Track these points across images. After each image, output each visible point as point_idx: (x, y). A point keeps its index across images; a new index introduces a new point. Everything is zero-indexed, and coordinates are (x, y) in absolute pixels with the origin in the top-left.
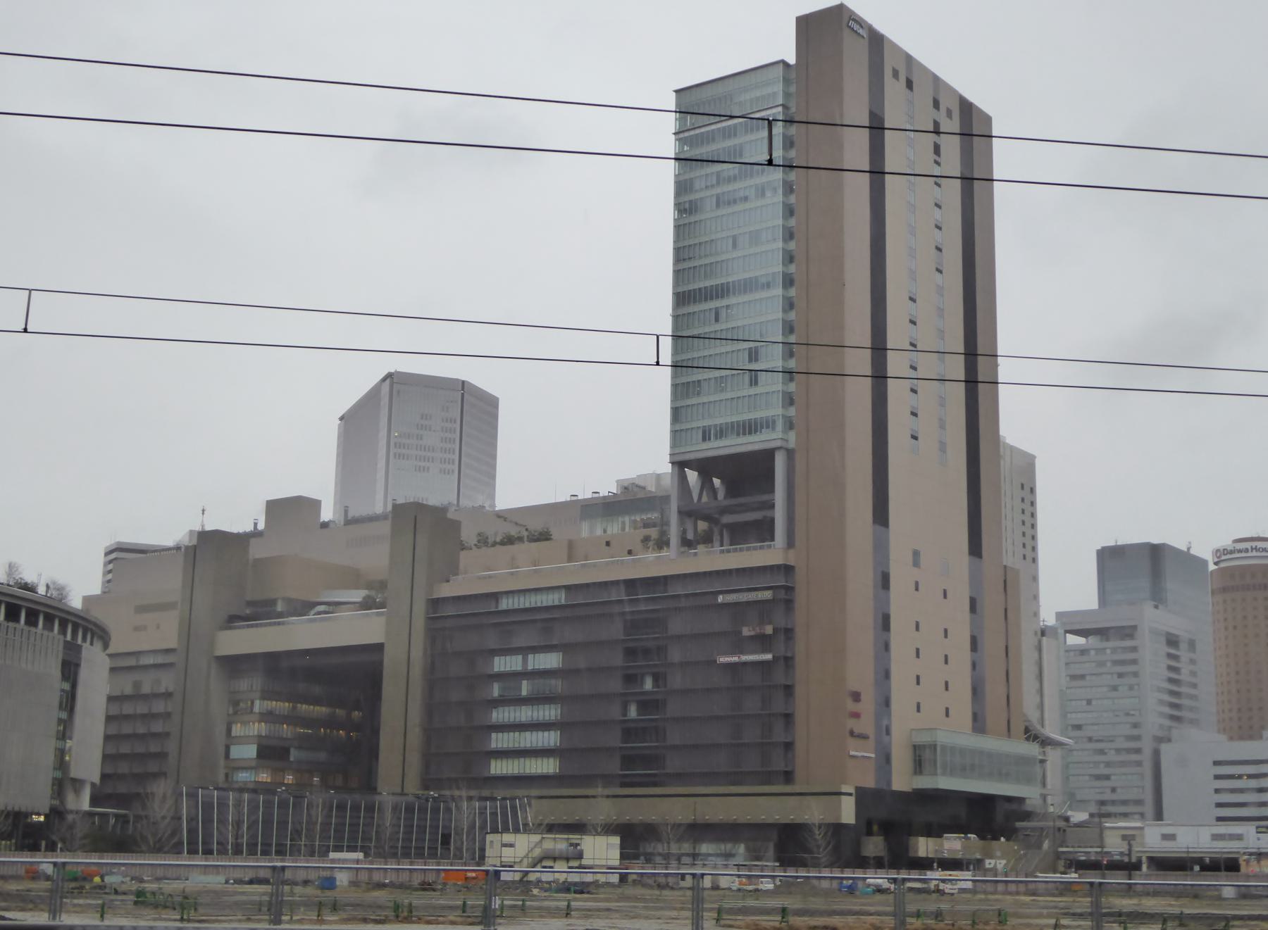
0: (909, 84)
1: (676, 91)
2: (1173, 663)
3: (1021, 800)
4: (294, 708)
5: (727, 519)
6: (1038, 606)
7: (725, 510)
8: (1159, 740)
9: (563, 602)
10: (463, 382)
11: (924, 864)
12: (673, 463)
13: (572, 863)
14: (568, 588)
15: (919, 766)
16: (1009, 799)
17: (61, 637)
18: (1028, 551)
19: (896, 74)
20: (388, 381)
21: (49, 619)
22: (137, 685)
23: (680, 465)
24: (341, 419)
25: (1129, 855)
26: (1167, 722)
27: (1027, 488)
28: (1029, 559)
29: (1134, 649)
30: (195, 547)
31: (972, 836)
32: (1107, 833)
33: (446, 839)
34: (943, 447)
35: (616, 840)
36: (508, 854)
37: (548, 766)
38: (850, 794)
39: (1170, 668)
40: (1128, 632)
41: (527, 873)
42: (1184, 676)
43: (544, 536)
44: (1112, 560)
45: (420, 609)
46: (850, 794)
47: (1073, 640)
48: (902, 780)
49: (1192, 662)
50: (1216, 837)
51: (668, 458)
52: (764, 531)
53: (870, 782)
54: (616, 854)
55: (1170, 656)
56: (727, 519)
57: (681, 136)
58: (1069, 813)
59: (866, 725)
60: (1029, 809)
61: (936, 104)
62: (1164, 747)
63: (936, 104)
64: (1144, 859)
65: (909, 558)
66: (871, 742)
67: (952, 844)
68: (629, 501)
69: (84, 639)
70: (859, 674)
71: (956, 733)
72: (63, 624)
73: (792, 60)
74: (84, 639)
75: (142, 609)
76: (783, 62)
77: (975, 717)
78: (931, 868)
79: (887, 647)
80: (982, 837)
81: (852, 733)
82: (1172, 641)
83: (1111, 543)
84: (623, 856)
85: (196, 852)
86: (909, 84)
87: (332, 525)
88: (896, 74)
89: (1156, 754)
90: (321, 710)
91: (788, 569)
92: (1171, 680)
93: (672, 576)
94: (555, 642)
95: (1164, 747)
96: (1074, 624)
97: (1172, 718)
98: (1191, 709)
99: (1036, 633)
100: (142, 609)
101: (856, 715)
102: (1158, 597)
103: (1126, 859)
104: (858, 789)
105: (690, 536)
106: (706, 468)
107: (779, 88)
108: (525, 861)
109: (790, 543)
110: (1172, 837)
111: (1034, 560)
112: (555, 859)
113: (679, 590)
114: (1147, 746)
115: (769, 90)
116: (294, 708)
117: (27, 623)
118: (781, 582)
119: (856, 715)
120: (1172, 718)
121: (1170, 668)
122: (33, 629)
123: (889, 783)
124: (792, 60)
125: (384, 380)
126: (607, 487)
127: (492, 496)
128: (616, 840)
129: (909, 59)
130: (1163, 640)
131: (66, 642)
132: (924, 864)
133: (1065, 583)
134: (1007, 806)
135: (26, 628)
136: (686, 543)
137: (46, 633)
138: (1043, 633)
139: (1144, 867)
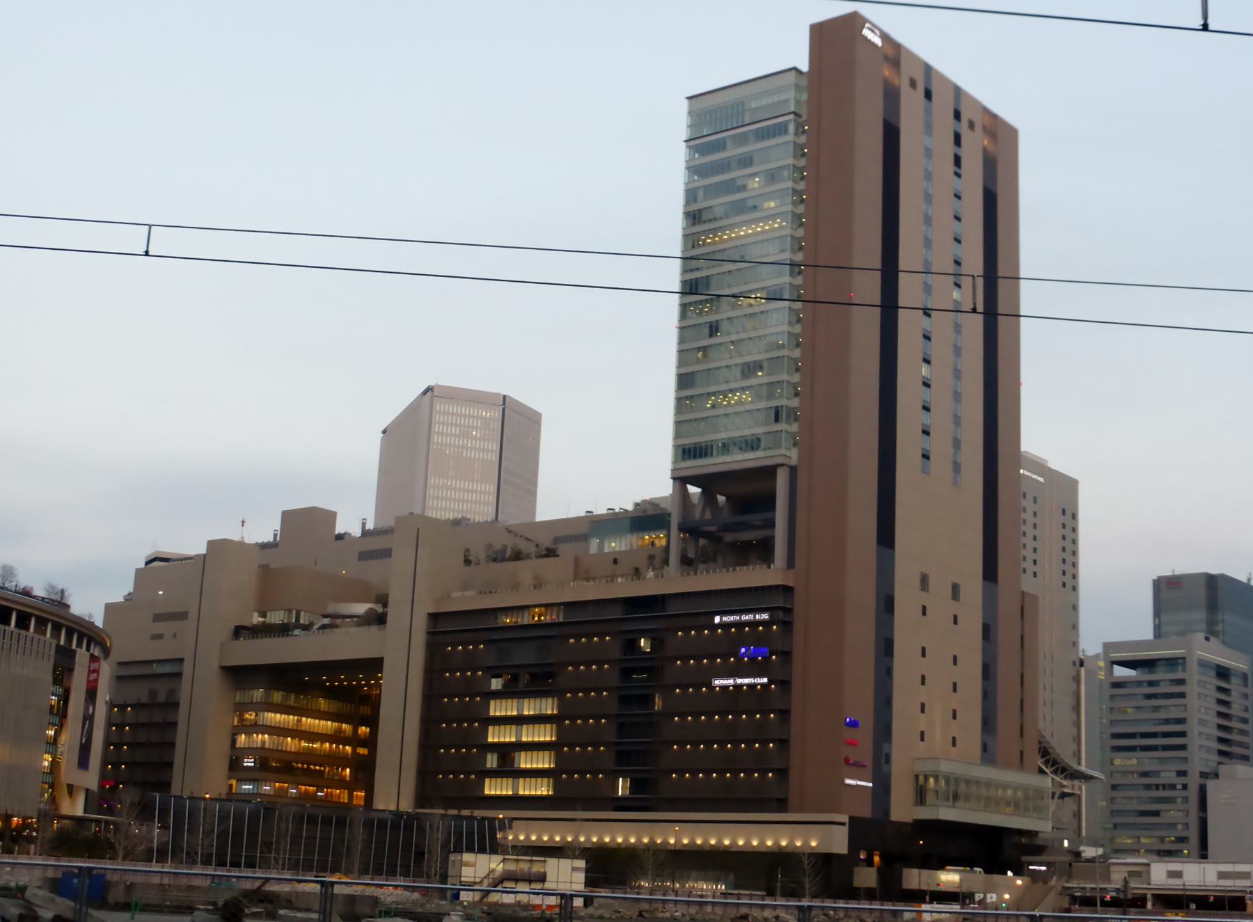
0: (928, 95)
1: (689, 98)
2: (1223, 697)
3: (1032, 834)
4: (299, 721)
5: (729, 537)
6: (1077, 635)
7: (726, 528)
8: (1203, 775)
9: (561, 620)
10: (505, 397)
11: (917, 896)
12: (674, 479)
13: (534, 886)
14: (569, 606)
15: (921, 796)
16: (1020, 833)
17: (54, 642)
18: (1068, 579)
19: (913, 84)
20: (429, 393)
21: (42, 622)
22: (153, 693)
23: (681, 481)
24: (384, 432)
25: (1125, 892)
26: (1216, 758)
27: (1069, 514)
28: (1069, 586)
29: (1181, 682)
30: (205, 556)
31: (978, 869)
32: (1113, 868)
33: (420, 855)
34: (957, 467)
35: (581, 864)
36: (467, 874)
37: (543, 789)
38: (843, 824)
39: (1220, 702)
40: (1173, 663)
41: (488, 892)
42: (1236, 710)
43: (550, 553)
44: (1169, 591)
45: (421, 624)
46: (843, 824)
47: (1120, 672)
48: (903, 810)
49: (1246, 696)
50: (1222, 875)
51: (669, 474)
52: (764, 551)
53: (865, 812)
54: (580, 877)
55: (1220, 689)
56: (729, 537)
57: (692, 143)
58: (1082, 848)
59: (864, 753)
60: (1040, 842)
61: (957, 115)
62: (1211, 784)
63: (957, 115)
64: (1149, 896)
65: (917, 581)
66: (869, 770)
67: (949, 878)
68: (646, 518)
69: (79, 645)
70: (859, 702)
71: (963, 762)
72: (57, 628)
73: (805, 67)
74: (79, 645)
75: (158, 618)
76: (795, 69)
77: (985, 748)
78: (924, 902)
79: (889, 672)
80: (987, 871)
81: (847, 761)
82: (1223, 673)
83: (1167, 572)
84: (589, 882)
85: (194, 862)
86: (928, 95)
87: (346, 537)
88: (913, 84)
89: (1203, 791)
90: (328, 726)
91: (787, 590)
92: (1220, 714)
93: (670, 595)
94: (551, 661)
95: (1211, 784)
96: (1118, 655)
97: (1221, 753)
98: (1241, 744)
99: (1074, 663)
100: (158, 618)
101: (852, 743)
102: (1211, 632)
103: (1122, 896)
104: (851, 818)
105: (691, 555)
106: (708, 482)
107: (791, 95)
108: (486, 882)
109: (791, 563)
110: (1178, 875)
111: (1075, 588)
112: (516, 880)
113: (673, 609)
114: (1194, 781)
115: (782, 97)
116: (299, 721)
117: (17, 626)
118: (780, 603)
119: (852, 743)
120: (1221, 753)
121: (1220, 702)
122: (23, 632)
123: (887, 813)
124: (805, 67)
125: (425, 393)
126: (625, 502)
127: (534, 514)
128: (581, 864)
129: (928, 69)
130: (1213, 673)
131: (58, 647)
132: (917, 896)
133: (1111, 608)
134: (1016, 839)
135: (16, 631)
136: (686, 561)
137: (37, 636)
138: (1082, 664)
139: (1149, 905)
